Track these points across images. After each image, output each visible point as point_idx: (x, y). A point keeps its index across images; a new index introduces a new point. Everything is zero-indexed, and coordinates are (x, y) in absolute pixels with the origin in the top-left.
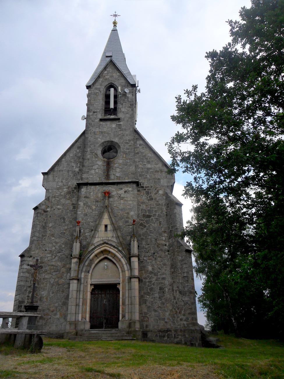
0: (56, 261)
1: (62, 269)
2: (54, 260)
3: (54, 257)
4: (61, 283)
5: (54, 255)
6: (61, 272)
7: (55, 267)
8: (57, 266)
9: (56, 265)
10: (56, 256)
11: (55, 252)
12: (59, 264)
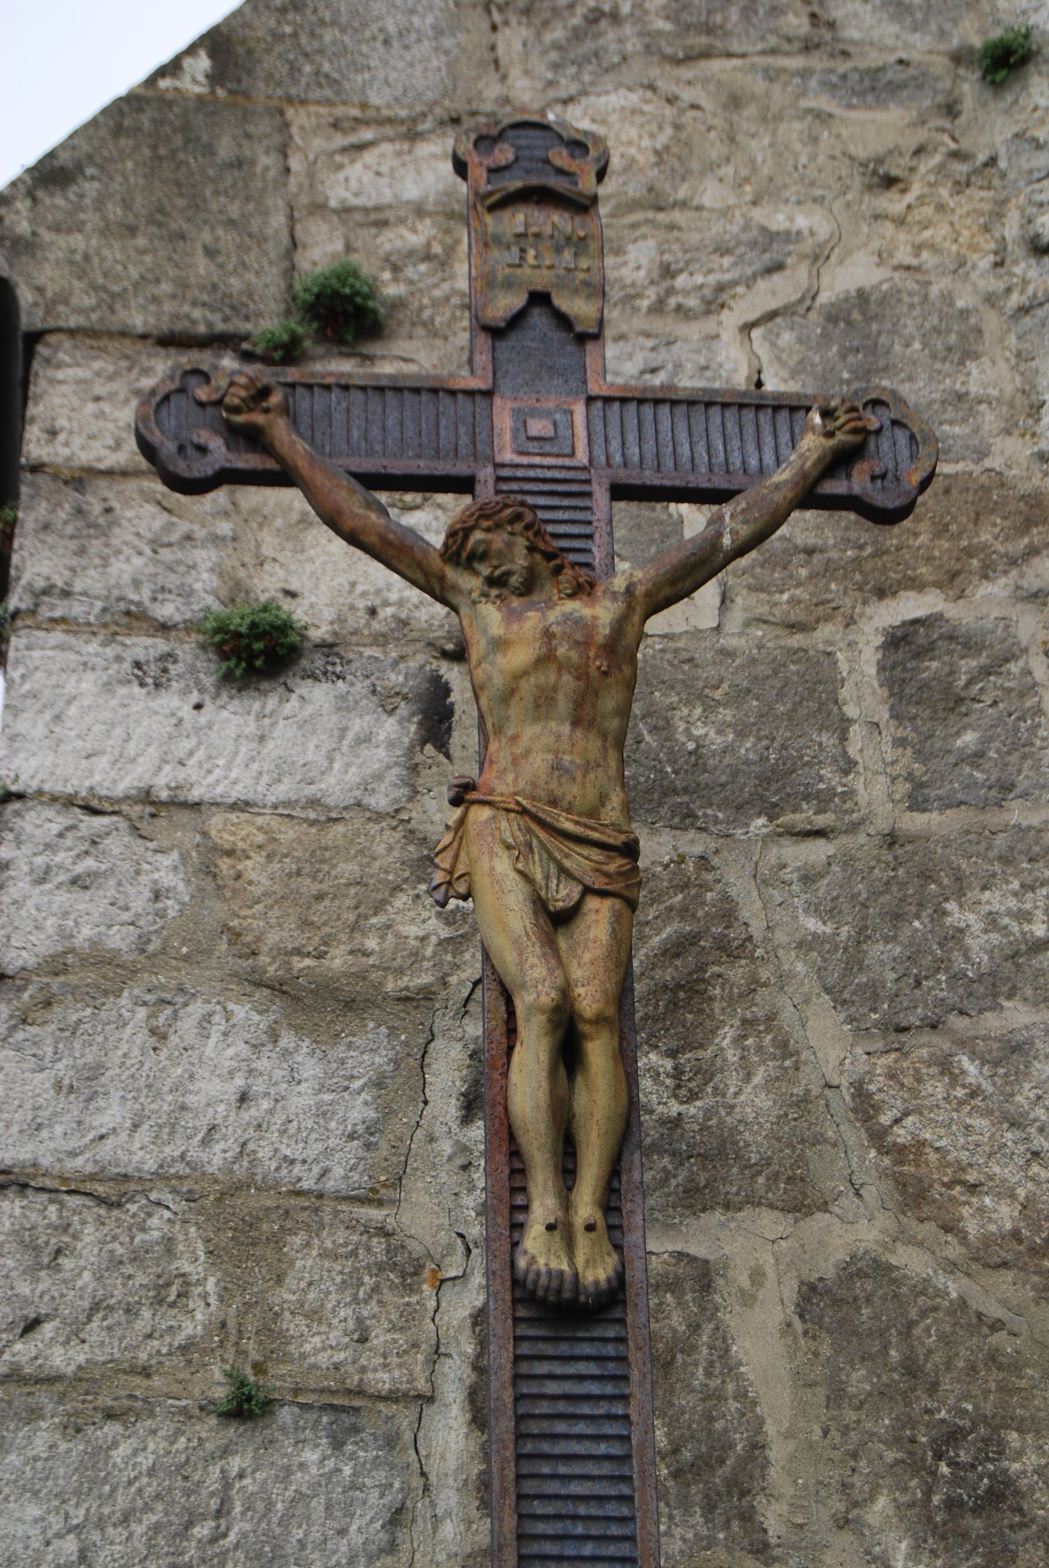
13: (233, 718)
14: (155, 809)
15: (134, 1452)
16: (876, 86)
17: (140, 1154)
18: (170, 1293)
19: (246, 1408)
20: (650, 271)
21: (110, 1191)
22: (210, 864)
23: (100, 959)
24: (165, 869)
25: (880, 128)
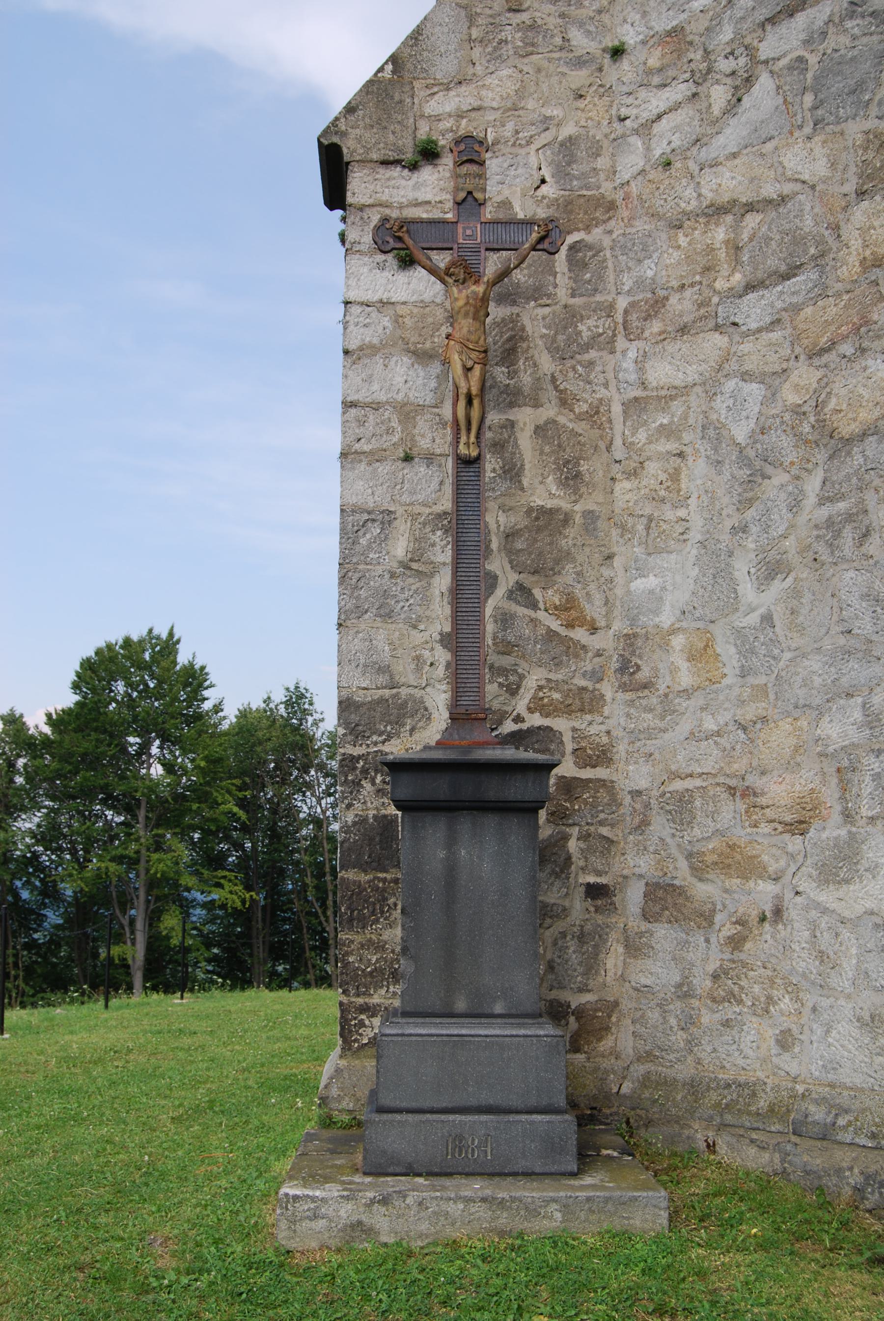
0: (758, 140)
1: (860, 213)
2: (731, 136)
3: (719, 95)
4: (866, 415)
5: (725, 65)
6: (849, 266)
7: (752, 220)
8: (783, 199)
9: (770, 191)
10: (749, 81)
11: (727, 34)
12: (807, 159)
13: (402, 277)
14: (384, 304)
15: (383, 469)
16: (580, 62)
17: (382, 397)
18: (389, 431)
19: (408, 458)
20: (596, 415)
21: (376, 406)
22: (397, 320)
23: (372, 346)
24: (386, 322)
25: (579, 77)
